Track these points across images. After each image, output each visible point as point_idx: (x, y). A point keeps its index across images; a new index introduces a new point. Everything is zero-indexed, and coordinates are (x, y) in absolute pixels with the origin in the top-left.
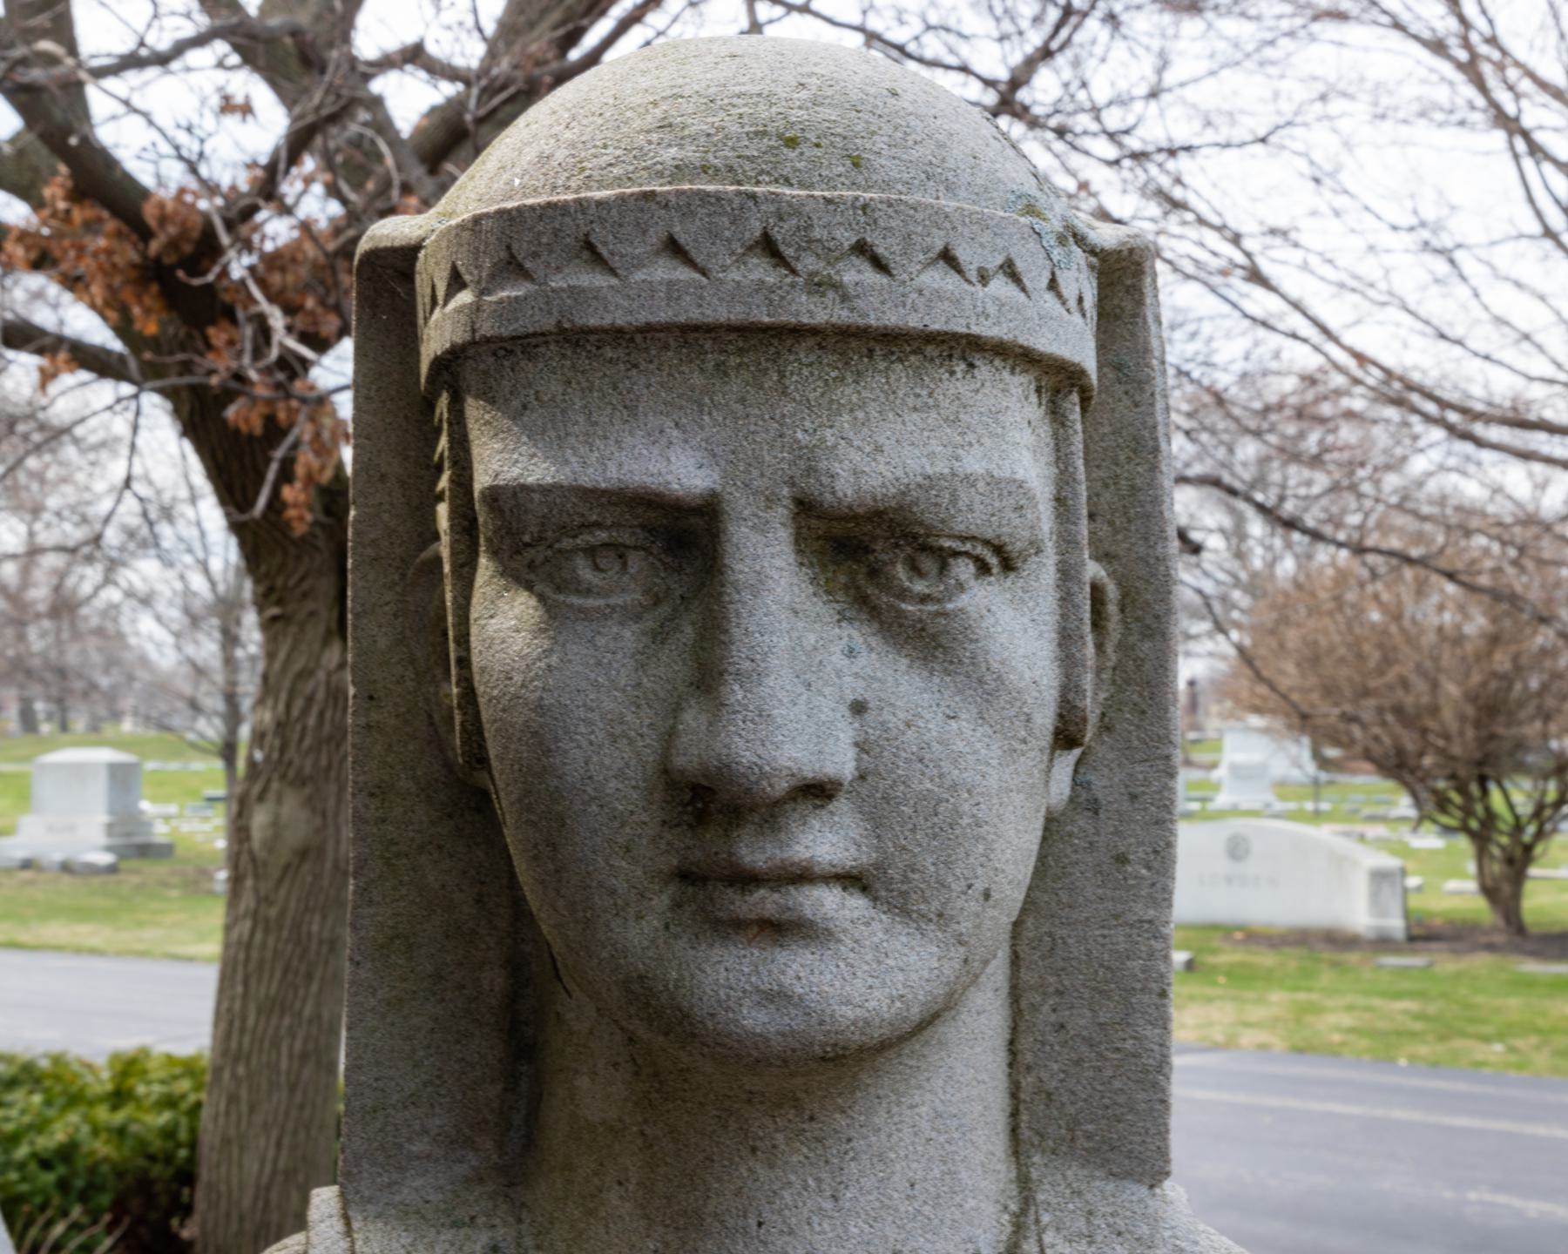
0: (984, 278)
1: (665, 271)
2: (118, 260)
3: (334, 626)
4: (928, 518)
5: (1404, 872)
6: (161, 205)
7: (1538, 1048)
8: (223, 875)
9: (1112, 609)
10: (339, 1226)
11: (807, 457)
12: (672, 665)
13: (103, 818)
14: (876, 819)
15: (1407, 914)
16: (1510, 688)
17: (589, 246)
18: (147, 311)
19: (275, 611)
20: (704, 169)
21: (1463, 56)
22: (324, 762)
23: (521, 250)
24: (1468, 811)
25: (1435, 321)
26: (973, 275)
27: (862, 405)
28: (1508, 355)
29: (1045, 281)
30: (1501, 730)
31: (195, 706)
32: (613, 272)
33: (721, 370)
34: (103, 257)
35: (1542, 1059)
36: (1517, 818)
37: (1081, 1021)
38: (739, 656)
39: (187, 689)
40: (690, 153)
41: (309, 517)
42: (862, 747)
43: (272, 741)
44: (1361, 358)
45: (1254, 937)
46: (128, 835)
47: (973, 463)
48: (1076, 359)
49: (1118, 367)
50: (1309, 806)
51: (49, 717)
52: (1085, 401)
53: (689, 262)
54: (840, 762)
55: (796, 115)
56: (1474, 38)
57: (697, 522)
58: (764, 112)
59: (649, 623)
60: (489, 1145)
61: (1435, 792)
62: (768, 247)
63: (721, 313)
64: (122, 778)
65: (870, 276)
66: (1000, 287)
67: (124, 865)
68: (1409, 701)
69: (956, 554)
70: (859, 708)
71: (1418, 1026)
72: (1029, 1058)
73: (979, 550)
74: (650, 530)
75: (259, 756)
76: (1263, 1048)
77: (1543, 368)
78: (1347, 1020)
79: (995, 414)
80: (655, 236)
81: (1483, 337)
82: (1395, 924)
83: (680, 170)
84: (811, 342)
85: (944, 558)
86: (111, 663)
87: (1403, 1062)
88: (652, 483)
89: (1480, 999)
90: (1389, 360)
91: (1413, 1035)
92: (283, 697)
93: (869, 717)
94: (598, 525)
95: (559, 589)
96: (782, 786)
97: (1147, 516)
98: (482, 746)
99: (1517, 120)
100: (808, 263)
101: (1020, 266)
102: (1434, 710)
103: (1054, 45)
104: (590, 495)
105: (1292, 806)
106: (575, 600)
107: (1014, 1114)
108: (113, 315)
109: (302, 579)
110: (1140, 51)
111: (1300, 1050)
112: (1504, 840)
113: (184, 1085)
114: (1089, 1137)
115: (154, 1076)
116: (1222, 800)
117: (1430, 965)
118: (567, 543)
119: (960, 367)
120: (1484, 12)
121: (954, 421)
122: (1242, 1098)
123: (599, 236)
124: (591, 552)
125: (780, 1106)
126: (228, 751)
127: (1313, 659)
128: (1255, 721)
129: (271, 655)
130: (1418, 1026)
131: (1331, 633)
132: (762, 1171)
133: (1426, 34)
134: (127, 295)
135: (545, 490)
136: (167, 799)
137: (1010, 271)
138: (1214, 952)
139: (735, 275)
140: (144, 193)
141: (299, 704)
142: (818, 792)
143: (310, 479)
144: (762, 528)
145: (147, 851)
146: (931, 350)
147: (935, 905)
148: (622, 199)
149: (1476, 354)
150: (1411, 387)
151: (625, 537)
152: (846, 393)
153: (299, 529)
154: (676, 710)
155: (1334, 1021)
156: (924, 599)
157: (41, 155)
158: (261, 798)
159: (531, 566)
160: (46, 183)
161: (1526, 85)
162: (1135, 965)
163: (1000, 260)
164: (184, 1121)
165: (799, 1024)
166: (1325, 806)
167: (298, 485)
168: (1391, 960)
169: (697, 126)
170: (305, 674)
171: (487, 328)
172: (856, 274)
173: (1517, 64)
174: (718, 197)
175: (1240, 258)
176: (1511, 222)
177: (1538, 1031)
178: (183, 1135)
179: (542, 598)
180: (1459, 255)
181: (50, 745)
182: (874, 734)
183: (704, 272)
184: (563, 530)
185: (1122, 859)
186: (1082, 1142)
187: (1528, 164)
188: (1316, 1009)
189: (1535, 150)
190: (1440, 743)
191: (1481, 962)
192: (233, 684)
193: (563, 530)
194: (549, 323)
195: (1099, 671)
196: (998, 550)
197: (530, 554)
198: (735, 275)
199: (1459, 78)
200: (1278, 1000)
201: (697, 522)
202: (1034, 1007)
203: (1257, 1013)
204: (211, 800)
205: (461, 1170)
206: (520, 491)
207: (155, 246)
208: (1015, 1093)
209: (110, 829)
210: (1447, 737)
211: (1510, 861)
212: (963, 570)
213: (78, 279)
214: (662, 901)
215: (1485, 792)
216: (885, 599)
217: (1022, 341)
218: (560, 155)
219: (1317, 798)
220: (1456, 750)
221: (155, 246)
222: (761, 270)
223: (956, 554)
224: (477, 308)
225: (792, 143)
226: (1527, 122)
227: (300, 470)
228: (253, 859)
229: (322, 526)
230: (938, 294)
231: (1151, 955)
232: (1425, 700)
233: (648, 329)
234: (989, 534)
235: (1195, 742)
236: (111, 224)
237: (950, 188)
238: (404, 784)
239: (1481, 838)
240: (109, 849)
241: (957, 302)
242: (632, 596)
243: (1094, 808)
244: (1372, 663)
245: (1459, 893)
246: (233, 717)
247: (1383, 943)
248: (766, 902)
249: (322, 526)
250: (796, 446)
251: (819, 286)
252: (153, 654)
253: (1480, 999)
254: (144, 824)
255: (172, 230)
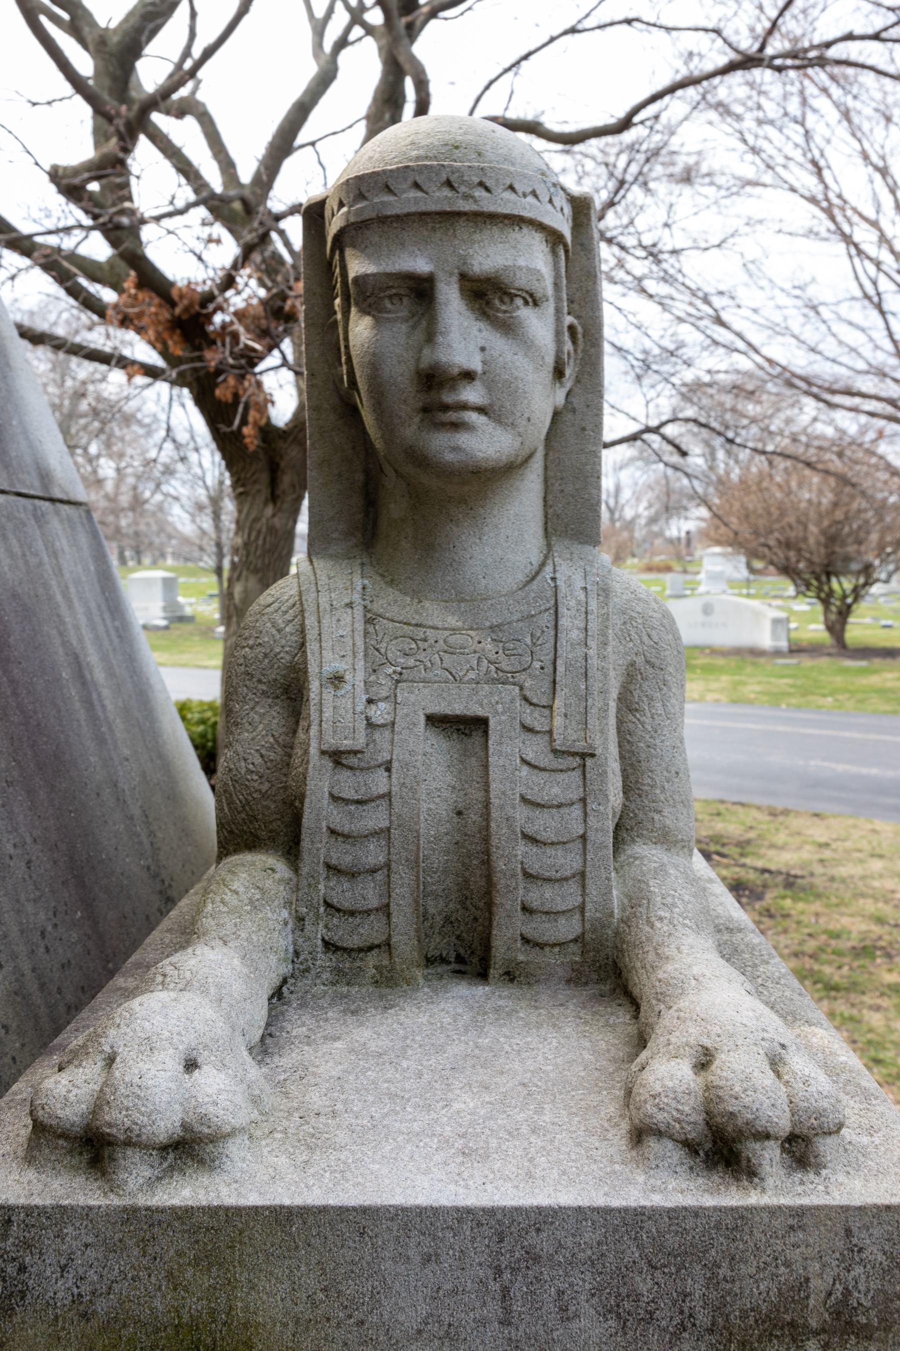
0: (525, 196)
1: (414, 194)
2: (161, 318)
3: (269, 496)
4: (506, 281)
5: (788, 620)
6: (180, 290)
7: (849, 699)
8: (221, 629)
9: (580, 336)
10: (308, 563)
11: (464, 260)
12: (419, 335)
13: (160, 604)
14: (490, 388)
15: (789, 640)
16: (842, 529)
17: (387, 187)
18: (175, 343)
19: (241, 490)
20: (427, 157)
21: (825, 204)
22: (267, 561)
23: (363, 189)
24: (820, 589)
25: (808, 342)
26: (521, 194)
27: (482, 241)
28: (844, 359)
29: (547, 199)
30: (837, 549)
31: (201, 549)
32: (395, 195)
33: (434, 229)
34: (153, 317)
35: (850, 704)
36: (844, 591)
37: (569, 488)
38: (441, 327)
39: (197, 541)
40: (422, 152)
41: (256, 442)
42: (484, 362)
43: (243, 552)
44: (770, 361)
45: (714, 652)
46: (173, 611)
47: (521, 262)
48: (560, 229)
49: (582, 245)
50: (744, 591)
51: (132, 559)
52: (566, 252)
53: (422, 190)
54: (476, 364)
55: (459, 138)
56: (831, 196)
57: (426, 285)
58: (447, 137)
59: (411, 323)
60: (359, 535)
61: (804, 580)
62: (449, 184)
63: (432, 207)
64: (169, 585)
65: (484, 194)
66: (530, 199)
67: (172, 626)
68: (793, 535)
69: (517, 296)
70: (483, 349)
71: (792, 690)
72: (551, 503)
73: (524, 294)
74: (411, 289)
75: (236, 559)
76: (717, 701)
77: (861, 365)
78: (758, 688)
79: (530, 246)
80: (410, 181)
81: (829, 347)
82: (784, 644)
83: (418, 158)
84: (464, 218)
85: (512, 297)
86: (161, 530)
87: (784, 706)
88: (411, 269)
89: (823, 678)
90: (783, 362)
91: (789, 694)
92: (247, 531)
93: (487, 352)
94: (392, 287)
95: (379, 312)
96: (456, 371)
97: (593, 301)
98: (354, 373)
99: (851, 236)
100: (463, 189)
101: (538, 192)
102: (805, 539)
103: (617, 199)
104: (389, 275)
105: (736, 591)
106: (385, 315)
107: (546, 523)
108: (159, 345)
109: (253, 474)
110: (660, 203)
111: (734, 702)
112: (838, 603)
113: (209, 714)
114: (572, 530)
115: (195, 710)
116: (702, 589)
117: (799, 663)
118: (382, 295)
119: (517, 228)
120: (836, 182)
121: (515, 247)
122: (706, 722)
123: (391, 183)
124: (390, 297)
125: (459, 503)
126: (219, 571)
127: (746, 516)
128: (717, 549)
129: (240, 511)
130: (792, 690)
131: (752, 502)
132: (455, 529)
133: (807, 194)
134: (166, 335)
135: (374, 275)
136: (190, 596)
137: (534, 194)
138: (695, 658)
139: (437, 194)
140: (172, 284)
141: (254, 534)
142: (468, 376)
143: (256, 423)
144: (448, 284)
145: (182, 619)
146: (506, 221)
147: (511, 420)
148: (398, 169)
149: (828, 359)
150: (794, 375)
151: (402, 292)
152: (477, 237)
153: (252, 448)
154: (420, 351)
155: (752, 689)
156: (505, 312)
157: (122, 265)
158: (238, 579)
159: (370, 306)
160: (125, 281)
161: (855, 219)
162: (588, 467)
163: (530, 190)
164: (210, 730)
165: (464, 458)
166: (752, 591)
167: (250, 426)
168: (781, 661)
169: (423, 143)
170: (256, 520)
171: (352, 219)
172: (479, 193)
173: (855, 210)
174: (431, 166)
175: (710, 311)
176: (848, 291)
177: (850, 692)
178: (210, 736)
179: (374, 316)
180: (821, 309)
181: (134, 570)
182: (488, 358)
183: (427, 193)
184: (381, 290)
185: (584, 429)
186: (570, 532)
187: (857, 260)
188: (744, 684)
189: (860, 252)
190: (807, 555)
191: (824, 661)
192: (219, 538)
193: (381, 290)
194: (374, 215)
195: (576, 359)
196: (531, 295)
197: (369, 300)
198: (437, 194)
199: (823, 216)
200: (725, 678)
201: (426, 285)
202: (553, 485)
203: (714, 685)
204: (212, 596)
205: (350, 543)
206: (365, 277)
207: (178, 311)
208: (546, 517)
209: (165, 609)
210: (811, 553)
211: (840, 613)
212: (519, 302)
213: (142, 328)
214: (417, 420)
215: (829, 580)
216: (491, 312)
217: (539, 219)
218: (377, 156)
219: (748, 587)
220: (816, 559)
221: (178, 311)
222: (446, 192)
223: (517, 296)
224: (349, 212)
225: (457, 147)
226: (856, 238)
227: (251, 419)
228: (236, 608)
229: (262, 448)
230: (508, 201)
231: (594, 463)
232: (801, 534)
233: (408, 215)
234: (528, 288)
235: (690, 562)
236: (157, 300)
237: (513, 164)
238: (326, 406)
239: (826, 602)
240: (165, 618)
241: (515, 203)
242: (404, 313)
243: (574, 411)
244: (774, 517)
245: (816, 631)
246: (220, 555)
247: (777, 653)
248: (452, 416)
249: (262, 448)
250: (460, 255)
251: (466, 197)
252: (180, 527)
253: (823, 678)
254: (180, 607)
255: (185, 302)
